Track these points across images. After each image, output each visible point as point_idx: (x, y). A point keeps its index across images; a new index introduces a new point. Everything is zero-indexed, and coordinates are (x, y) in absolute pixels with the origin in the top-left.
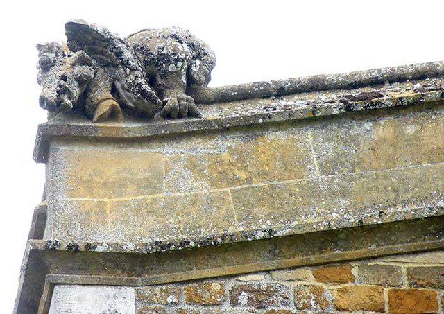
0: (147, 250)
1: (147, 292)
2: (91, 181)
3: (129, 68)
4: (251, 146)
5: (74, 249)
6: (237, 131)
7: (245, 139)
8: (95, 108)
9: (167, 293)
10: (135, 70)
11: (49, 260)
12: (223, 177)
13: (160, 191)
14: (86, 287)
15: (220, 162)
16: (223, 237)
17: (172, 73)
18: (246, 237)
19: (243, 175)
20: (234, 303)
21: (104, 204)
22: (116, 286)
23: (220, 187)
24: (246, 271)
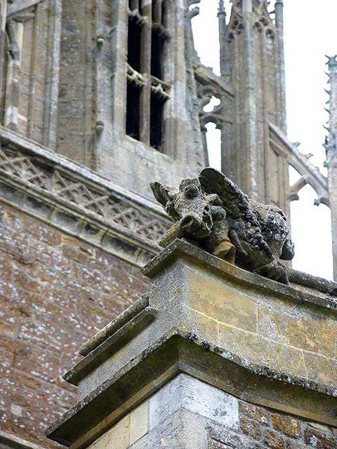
0: (258, 371)
1: (247, 407)
2: (206, 302)
3: (251, 222)
4: (316, 323)
5: (206, 348)
6: (308, 307)
7: (313, 316)
8: (217, 244)
9: (261, 414)
10: (256, 226)
11: (183, 349)
12: (297, 339)
13: (255, 331)
14: (203, 384)
15: (296, 326)
16: (311, 383)
17: (276, 241)
18: (327, 391)
19: (312, 344)
20: (308, 442)
21: (216, 324)
22: (225, 392)
23: (296, 346)
24: (312, 418)
